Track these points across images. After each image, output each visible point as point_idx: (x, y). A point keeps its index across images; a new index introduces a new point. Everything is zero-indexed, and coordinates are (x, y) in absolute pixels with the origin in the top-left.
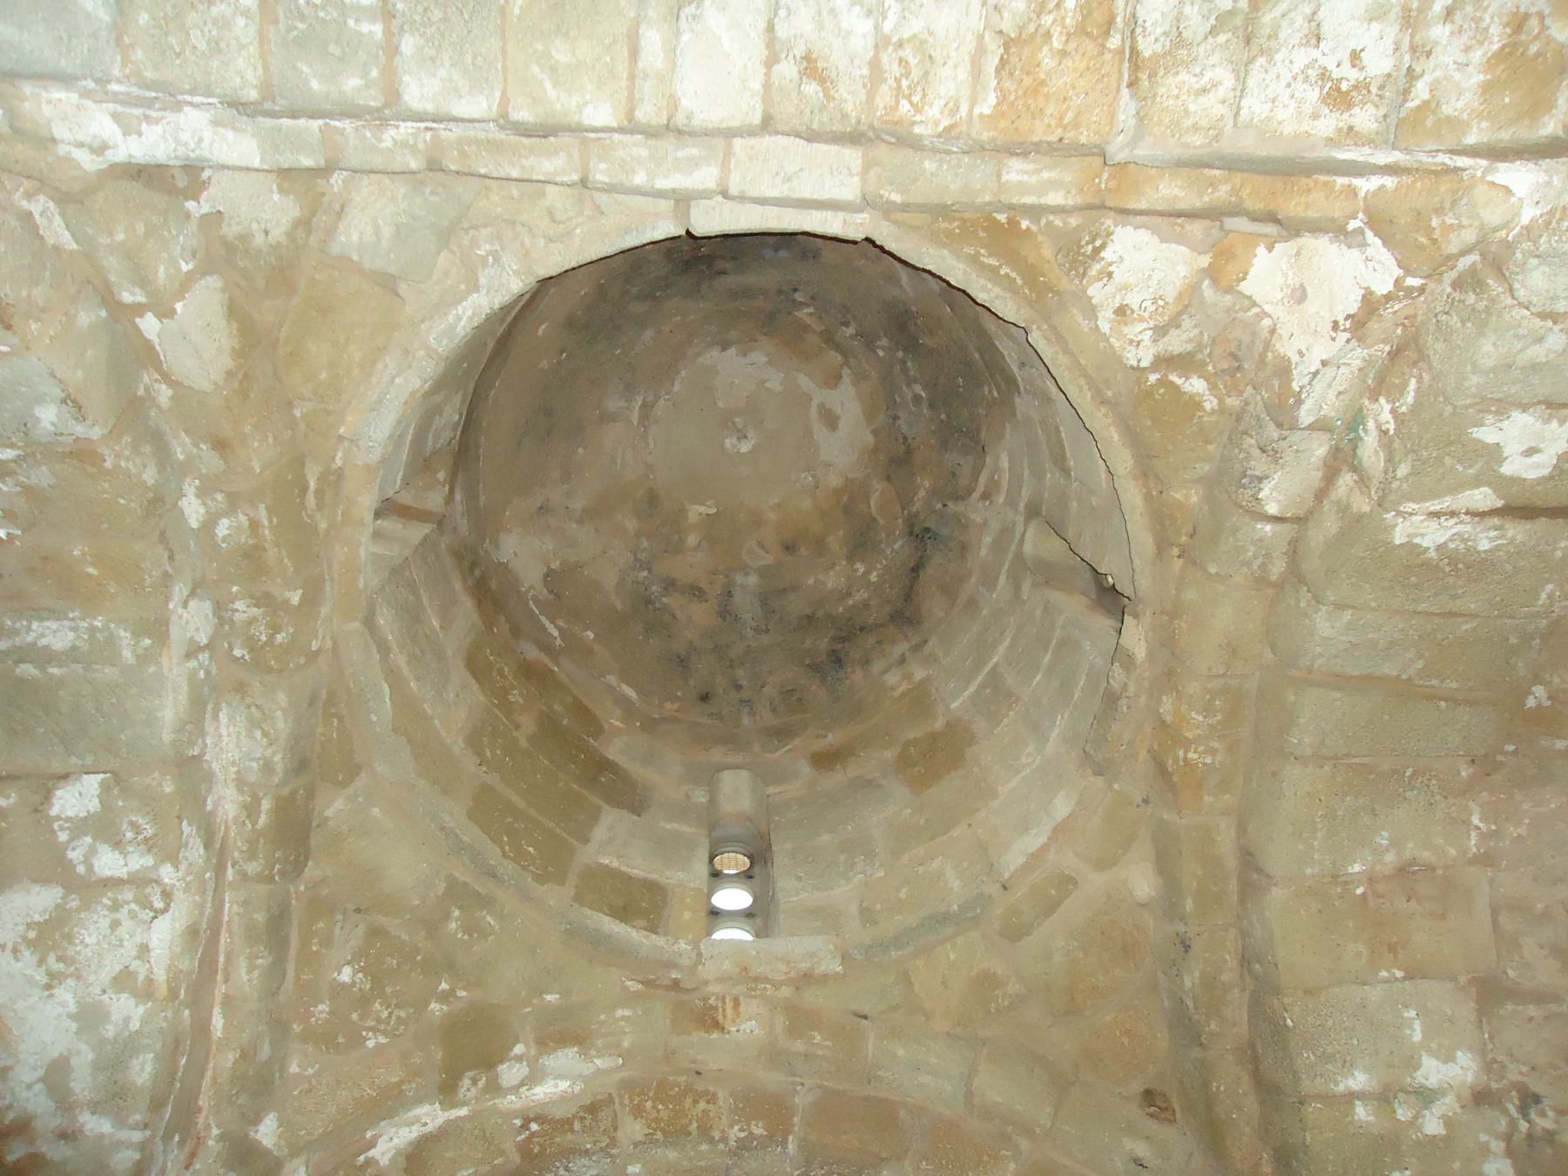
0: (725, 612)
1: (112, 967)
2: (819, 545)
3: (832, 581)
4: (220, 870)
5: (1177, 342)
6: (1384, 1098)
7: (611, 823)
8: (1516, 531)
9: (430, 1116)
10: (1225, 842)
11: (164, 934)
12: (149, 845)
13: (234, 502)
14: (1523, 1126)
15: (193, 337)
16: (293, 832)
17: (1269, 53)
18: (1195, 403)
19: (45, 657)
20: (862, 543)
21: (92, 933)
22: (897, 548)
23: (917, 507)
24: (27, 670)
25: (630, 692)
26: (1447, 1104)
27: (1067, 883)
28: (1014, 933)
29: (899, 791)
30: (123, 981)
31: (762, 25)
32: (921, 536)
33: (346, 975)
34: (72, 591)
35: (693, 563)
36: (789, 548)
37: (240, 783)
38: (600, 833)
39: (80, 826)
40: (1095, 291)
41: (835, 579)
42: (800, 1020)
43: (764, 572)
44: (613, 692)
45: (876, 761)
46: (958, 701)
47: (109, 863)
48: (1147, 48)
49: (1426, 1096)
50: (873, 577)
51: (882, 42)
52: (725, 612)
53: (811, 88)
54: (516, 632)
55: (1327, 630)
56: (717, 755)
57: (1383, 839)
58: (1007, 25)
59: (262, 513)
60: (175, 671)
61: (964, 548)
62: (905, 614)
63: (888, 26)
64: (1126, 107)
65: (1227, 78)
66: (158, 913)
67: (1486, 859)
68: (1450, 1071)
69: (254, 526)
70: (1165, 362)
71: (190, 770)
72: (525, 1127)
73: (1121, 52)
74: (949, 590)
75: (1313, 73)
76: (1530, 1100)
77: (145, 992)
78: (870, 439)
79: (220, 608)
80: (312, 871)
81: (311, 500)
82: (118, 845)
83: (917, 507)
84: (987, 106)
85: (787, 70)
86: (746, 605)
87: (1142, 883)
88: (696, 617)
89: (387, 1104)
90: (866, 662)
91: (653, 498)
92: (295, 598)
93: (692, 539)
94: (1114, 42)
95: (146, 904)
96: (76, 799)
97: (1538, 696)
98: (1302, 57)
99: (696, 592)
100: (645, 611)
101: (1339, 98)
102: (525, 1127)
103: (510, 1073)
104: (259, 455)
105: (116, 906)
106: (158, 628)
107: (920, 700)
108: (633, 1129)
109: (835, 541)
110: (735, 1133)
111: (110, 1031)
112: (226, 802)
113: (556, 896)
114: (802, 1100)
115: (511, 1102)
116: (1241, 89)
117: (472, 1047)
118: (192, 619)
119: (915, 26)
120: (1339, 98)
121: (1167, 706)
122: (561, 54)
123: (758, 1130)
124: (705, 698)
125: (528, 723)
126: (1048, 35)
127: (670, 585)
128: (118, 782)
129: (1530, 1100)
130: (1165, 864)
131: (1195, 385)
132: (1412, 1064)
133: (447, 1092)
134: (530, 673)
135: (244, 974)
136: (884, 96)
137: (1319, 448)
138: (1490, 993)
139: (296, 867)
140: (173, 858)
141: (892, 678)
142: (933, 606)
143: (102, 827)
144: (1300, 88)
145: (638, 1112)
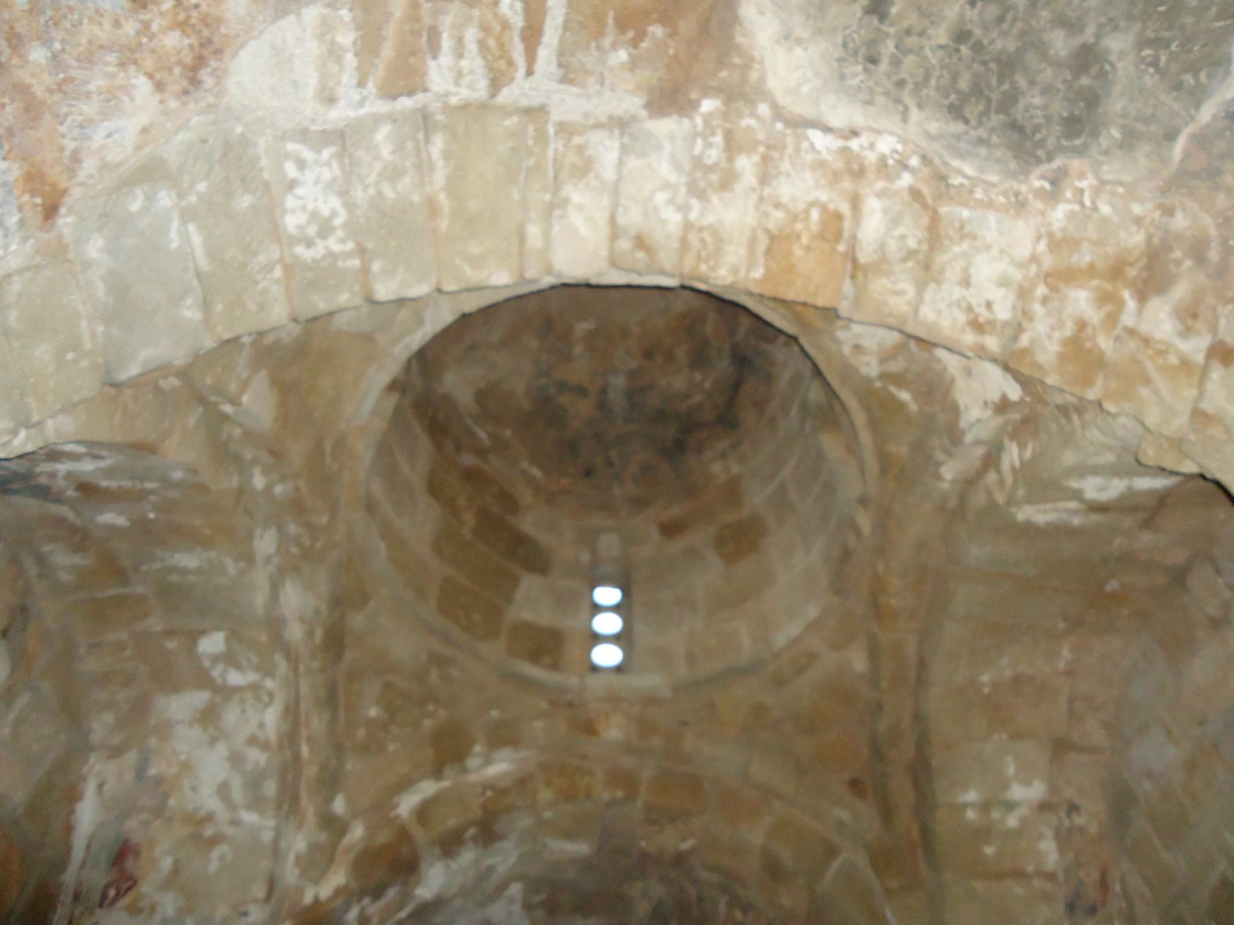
0: (603, 406)
1: (246, 732)
2: (669, 357)
3: (678, 383)
4: (295, 670)
5: (894, 367)
6: (985, 807)
7: (529, 585)
8: (1096, 518)
9: (428, 788)
10: (911, 647)
11: (271, 717)
12: (257, 669)
13: (283, 478)
14: (1067, 823)
15: (256, 403)
16: (335, 641)
17: (939, 283)
18: (901, 406)
19: (184, 572)
20: (699, 359)
21: (231, 715)
22: (723, 366)
23: (739, 337)
24: (174, 578)
25: (536, 472)
26: (1024, 811)
27: (812, 657)
28: (780, 682)
29: (714, 561)
30: (252, 741)
31: (607, 216)
32: (742, 360)
33: (373, 712)
34: (193, 539)
35: (579, 369)
36: (648, 355)
37: (302, 619)
38: (520, 594)
39: (216, 659)
40: (840, 334)
41: (678, 381)
42: (645, 727)
43: (631, 374)
44: (524, 473)
45: (700, 537)
46: (757, 498)
47: (235, 678)
48: (863, 258)
49: (1010, 806)
50: (707, 385)
51: (688, 226)
52: (603, 406)
53: (641, 255)
54: (459, 447)
55: (977, 552)
56: (597, 520)
57: (1005, 661)
58: (771, 225)
59: (302, 483)
60: (261, 578)
61: (769, 379)
62: (727, 420)
63: (693, 216)
64: (848, 287)
65: (910, 289)
66: (267, 705)
67: (1069, 673)
68: (1027, 794)
69: (297, 489)
70: (885, 376)
71: (274, 625)
72: (483, 793)
73: (845, 255)
74: (759, 406)
75: (964, 305)
76: (1073, 808)
77: (266, 746)
78: (739, 39)
79: (280, 529)
80: (349, 656)
81: (328, 460)
82: (239, 667)
83: (739, 337)
84: (758, 273)
85: (624, 244)
86: (616, 397)
87: (858, 662)
88: (581, 410)
89: (405, 784)
90: (699, 451)
91: (549, 323)
92: (324, 519)
93: (578, 349)
94: (841, 248)
95: (259, 700)
96: (212, 644)
97: (1112, 586)
98: (957, 292)
99: (581, 391)
100: (544, 412)
101: (977, 326)
102: (483, 793)
103: (472, 763)
104: (297, 452)
105: (243, 701)
106: (248, 557)
107: (733, 492)
108: (545, 795)
109: (681, 353)
110: (606, 796)
111: (249, 767)
112: (295, 632)
113: (494, 649)
114: (647, 773)
115: (473, 778)
116: (920, 299)
117: (449, 749)
118: (266, 543)
119: (710, 219)
120: (977, 326)
121: (880, 567)
122: (474, 249)
123: (620, 794)
124: (588, 473)
125: (469, 519)
126: (798, 236)
127: (563, 386)
128: (234, 636)
129: (1073, 808)
130: (874, 653)
131: (904, 396)
132: (1006, 787)
133: (437, 774)
134: (471, 476)
135: (317, 724)
136: (689, 261)
137: (980, 451)
138: (1061, 747)
139: (339, 657)
140: (269, 672)
141: (716, 468)
142: (748, 416)
143: (229, 659)
144: (955, 311)
145: (548, 784)
